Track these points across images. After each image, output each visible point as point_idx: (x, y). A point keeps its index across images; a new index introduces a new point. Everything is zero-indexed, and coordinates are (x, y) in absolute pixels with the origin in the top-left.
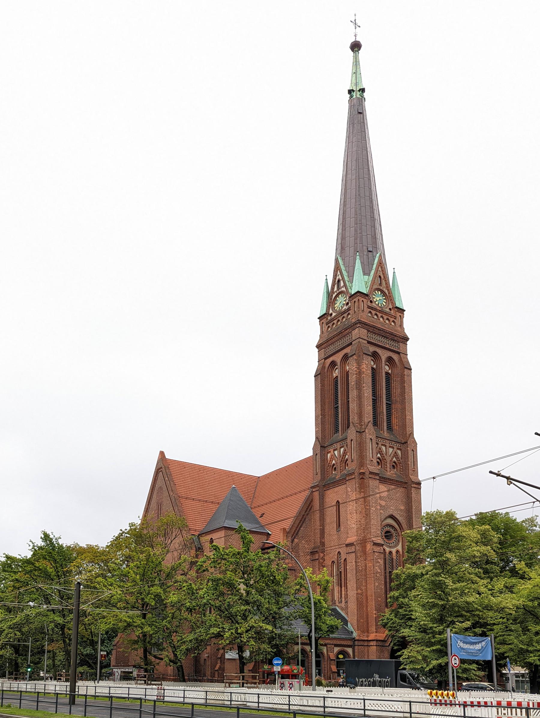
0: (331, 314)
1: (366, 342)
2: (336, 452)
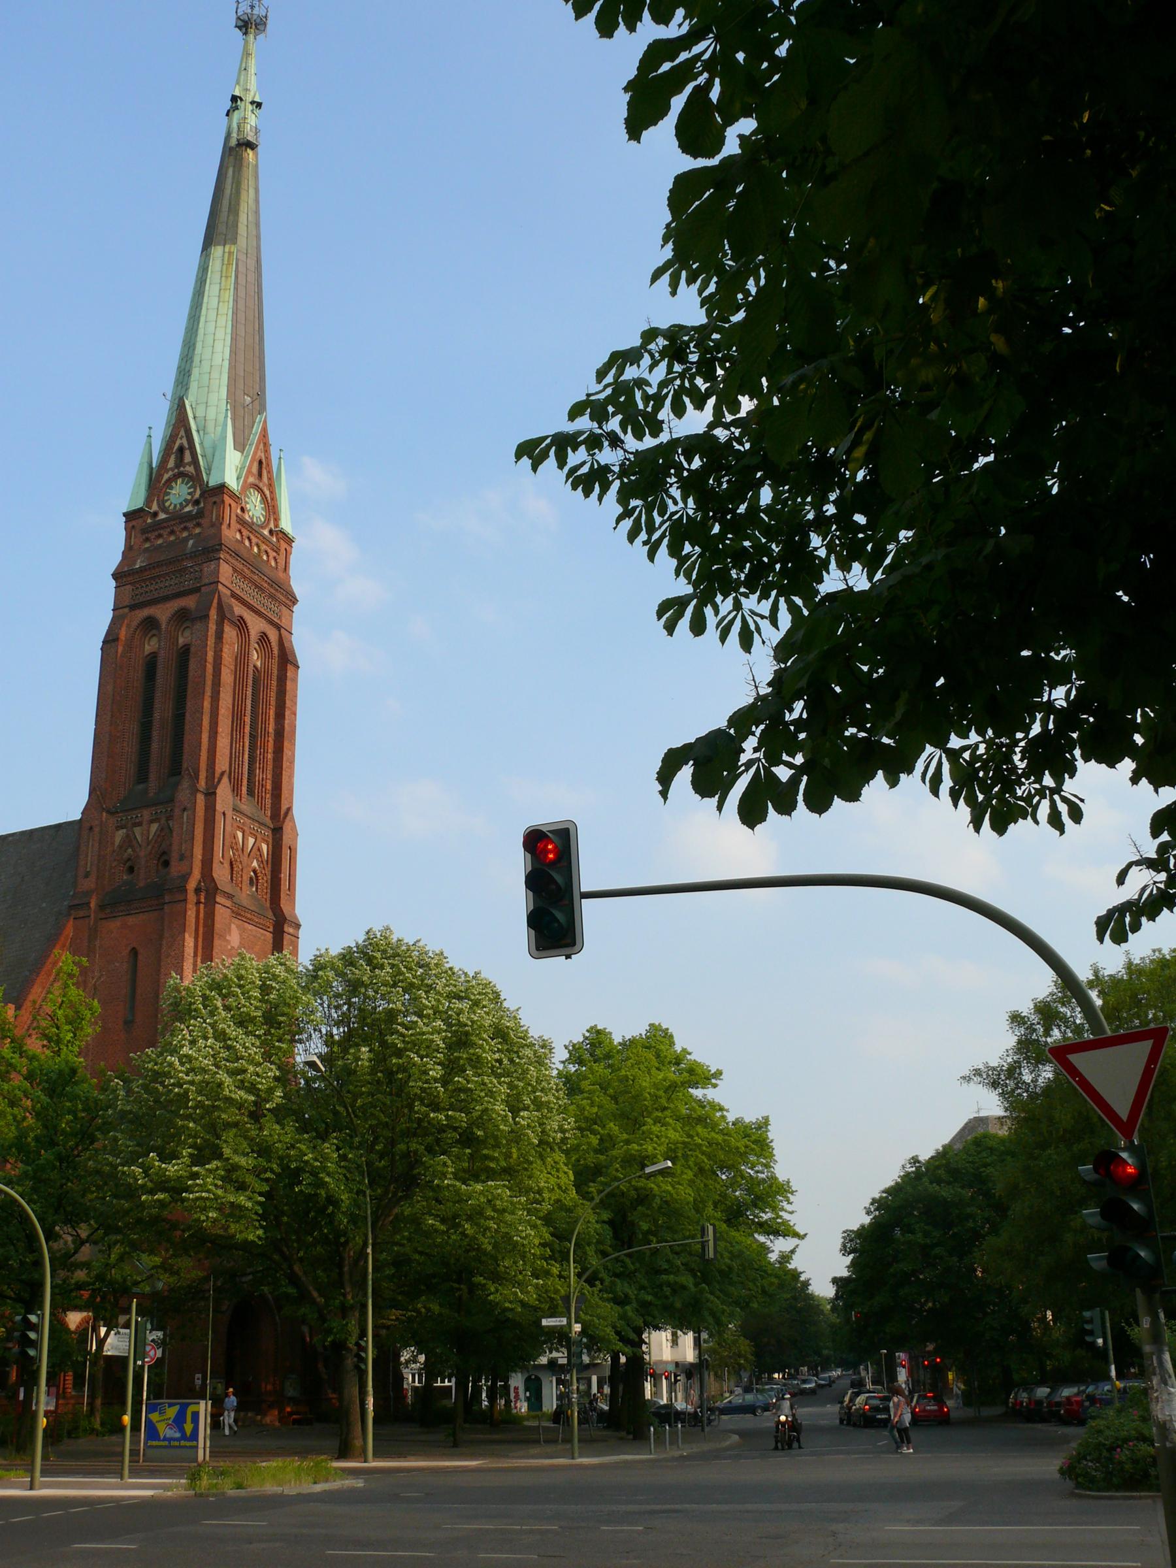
0: (155, 514)
1: (228, 593)
2: (137, 830)
